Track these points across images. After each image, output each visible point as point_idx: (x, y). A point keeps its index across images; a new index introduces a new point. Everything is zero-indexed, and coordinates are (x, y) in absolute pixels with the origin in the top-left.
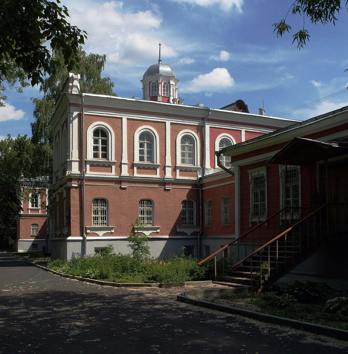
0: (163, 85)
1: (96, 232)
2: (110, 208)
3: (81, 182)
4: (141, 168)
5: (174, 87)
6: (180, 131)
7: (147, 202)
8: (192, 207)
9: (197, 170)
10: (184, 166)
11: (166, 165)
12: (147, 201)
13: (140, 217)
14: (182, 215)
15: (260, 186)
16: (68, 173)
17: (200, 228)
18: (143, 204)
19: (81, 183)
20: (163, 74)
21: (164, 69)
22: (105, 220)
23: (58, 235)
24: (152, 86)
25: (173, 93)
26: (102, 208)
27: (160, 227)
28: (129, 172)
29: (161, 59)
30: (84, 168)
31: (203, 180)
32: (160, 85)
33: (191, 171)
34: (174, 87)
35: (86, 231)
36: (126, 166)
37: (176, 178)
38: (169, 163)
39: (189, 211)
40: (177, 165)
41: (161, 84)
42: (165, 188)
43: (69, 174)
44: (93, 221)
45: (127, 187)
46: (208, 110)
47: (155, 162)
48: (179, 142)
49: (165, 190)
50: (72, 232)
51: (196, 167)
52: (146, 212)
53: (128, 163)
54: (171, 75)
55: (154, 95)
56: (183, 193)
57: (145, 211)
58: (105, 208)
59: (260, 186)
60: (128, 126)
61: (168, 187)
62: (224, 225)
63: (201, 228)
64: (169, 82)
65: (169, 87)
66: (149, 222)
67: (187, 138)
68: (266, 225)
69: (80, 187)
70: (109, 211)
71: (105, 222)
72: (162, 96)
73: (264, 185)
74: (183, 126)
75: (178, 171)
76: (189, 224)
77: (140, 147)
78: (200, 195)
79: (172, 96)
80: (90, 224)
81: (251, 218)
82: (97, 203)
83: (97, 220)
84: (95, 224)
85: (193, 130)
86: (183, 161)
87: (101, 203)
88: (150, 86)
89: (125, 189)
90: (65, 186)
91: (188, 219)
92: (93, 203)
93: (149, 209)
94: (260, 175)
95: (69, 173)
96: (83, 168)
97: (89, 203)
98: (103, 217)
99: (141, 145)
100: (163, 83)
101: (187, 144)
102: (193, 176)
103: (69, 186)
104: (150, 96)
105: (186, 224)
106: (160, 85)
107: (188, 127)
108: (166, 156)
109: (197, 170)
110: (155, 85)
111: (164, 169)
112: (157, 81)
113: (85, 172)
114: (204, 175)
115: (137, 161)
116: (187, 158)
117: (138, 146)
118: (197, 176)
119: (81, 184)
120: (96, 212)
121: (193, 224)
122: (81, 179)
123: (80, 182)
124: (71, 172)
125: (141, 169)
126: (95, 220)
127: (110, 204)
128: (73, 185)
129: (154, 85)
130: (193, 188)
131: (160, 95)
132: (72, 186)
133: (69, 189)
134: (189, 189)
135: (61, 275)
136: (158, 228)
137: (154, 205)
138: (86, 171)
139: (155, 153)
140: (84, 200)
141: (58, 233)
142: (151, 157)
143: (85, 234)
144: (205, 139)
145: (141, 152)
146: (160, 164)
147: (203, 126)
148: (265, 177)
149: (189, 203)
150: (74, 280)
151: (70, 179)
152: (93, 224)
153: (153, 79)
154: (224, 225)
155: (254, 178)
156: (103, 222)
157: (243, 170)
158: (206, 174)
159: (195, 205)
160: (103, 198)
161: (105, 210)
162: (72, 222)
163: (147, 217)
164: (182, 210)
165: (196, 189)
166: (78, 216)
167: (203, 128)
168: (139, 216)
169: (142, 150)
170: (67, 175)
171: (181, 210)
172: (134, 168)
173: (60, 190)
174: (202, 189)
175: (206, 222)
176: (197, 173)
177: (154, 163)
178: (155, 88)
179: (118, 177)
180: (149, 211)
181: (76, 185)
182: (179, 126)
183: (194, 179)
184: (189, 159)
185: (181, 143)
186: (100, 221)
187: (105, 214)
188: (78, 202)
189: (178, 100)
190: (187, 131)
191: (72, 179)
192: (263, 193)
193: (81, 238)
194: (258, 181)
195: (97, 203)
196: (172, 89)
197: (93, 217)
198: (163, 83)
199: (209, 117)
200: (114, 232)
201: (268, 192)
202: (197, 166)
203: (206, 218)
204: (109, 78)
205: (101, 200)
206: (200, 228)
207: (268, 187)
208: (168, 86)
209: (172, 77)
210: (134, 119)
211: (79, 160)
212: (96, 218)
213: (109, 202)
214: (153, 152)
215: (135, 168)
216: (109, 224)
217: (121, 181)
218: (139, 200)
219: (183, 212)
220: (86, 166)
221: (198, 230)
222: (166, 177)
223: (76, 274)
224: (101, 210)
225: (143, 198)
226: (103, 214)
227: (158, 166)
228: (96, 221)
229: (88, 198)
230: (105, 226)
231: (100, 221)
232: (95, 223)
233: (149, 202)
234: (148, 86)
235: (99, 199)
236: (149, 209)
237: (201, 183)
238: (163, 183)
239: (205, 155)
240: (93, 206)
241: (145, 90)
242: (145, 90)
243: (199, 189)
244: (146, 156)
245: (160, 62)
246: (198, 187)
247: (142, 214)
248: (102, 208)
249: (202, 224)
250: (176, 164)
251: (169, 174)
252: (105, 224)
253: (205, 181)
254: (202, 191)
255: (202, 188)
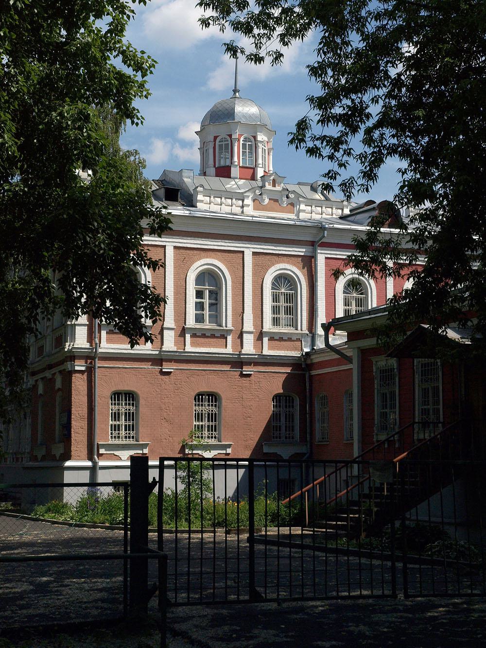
0: (241, 142)
1: (116, 453)
2: (141, 409)
3: (92, 362)
4: (197, 335)
5: (266, 145)
6: (270, 267)
7: (209, 398)
8: (293, 407)
9: (301, 338)
10: (277, 331)
11: (243, 330)
12: (209, 395)
13: (195, 425)
14: (274, 421)
15: (389, 383)
16: (67, 346)
17: (307, 445)
18: (202, 401)
19: (91, 363)
20: (243, 121)
21: (245, 109)
22: (133, 430)
23: (39, 457)
24: (221, 146)
25: (264, 158)
26: (126, 409)
27: (231, 443)
28: (176, 343)
29: (238, 88)
30: (97, 336)
31: (312, 357)
32: (236, 144)
33: (290, 340)
34: (266, 145)
35: (98, 451)
36: (172, 333)
37: (262, 353)
38: (249, 325)
39: (286, 414)
40: (264, 330)
41: (239, 140)
42: (241, 372)
43: (70, 348)
44: (110, 432)
45: (172, 370)
46: (321, 228)
47: (224, 325)
48: (268, 286)
49: (242, 375)
50: (72, 453)
51: (299, 331)
52: (206, 415)
53: (175, 327)
54: (259, 123)
55: (222, 164)
56: (274, 382)
57: (205, 414)
58: (132, 409)
59: (389, 383)
60: (176, 260)
61: (247, 370)
62: (348, 442)
63: (308, 446)
64: (255, 137)
65: (256, 147)
66: (212, 434)
67: (283, 279)
68: (386, 446)
69: (90, 372)
70: (141, 415)
71: (132, 434)
72: (240, 167)
73: (394, 383)
74: (275, 257)
75: (265, 340)
76: (286, 438)
77: (196, 298)
78: (307, 384)
79: (261, 166)
80: (103, 437)
81: (377, 435)
82: (119, 400)
83: (119, 430)
84: (115, 437)
85: (294, 265)
86: (276, 322)
87: (126, 400)
88: (215, 144)
89: (169, 373)
90: (61, 368)
91: (283, 428)
92: (112, 401)
93: (212, 411)
94: (388, 366)
95: (69, 346)
96: (95, 337)
97: (103, 399)
98: (129, 425)
99: (199, 294)
100: (242, 139)
101: (283, 291)
102: (295, 349)
103: (70, 369)
104: (215, 166)
105: (280, 438)
106: (236, 144)
107: (285, 258)
108: (243, 313)
109: (301, 338)
110: (226, 143)
111: (241, 336)
112: (230, 136)
113: (98, 344)
114: (315, 348)
115: (191, 323)
116: (282, 315)
117: (193, 297)
118: (302, 350)
119: (90, 365)
120: (116, 416)
121: (293, 438)
122: (90, 357)
123: (89, 361)
124: (73, 345)
125: (199, 337)
126: (115, 430)
127: (142, 402)
128: (77, 368)
129: (224, 143)
130: (293, 372)
131: (236, 163)
132: (76, 369)
133: (68, 376)
134: (287, 373)
135: (70, 525)
136: (229, 446)
137: (220, 403)
138: (100, 343)
139: (224, 308)
140: (97, 396)
141: (40, 453)
142: (217, 315)
143: (96, 457)
144: (316, 281)
145: (200, 306)
146: (232, 328)
147: (313, 257)
148: (396, 370)
149: (286, 399)
150: (97, 529)
151: (72, 356)
152: (110, 437)
153: (220, 130)
154: (348, 442)
155: (380, 370)
156: (129, 433)
157: (365, 355)
158: (318, 345)
159: (297, 402)
160: (130, 391)
161: (133, 413)
162: (73, 435)
163: (208, 426)
164: (273, 411)
165: (300, 372)
166: (84, 424)
167: (313, 260)
168: (195, 423)
169: (200, 303)
170: (66, 350)
171: (271, 413)
172: (185, 335)
173: (48, 374)
174: (310, 373)
175: (318, 436)
176: (302, 344)
177: (221, 326)
178: (228, 147)
179: (157, 352)
180: (212, 414)
181: (83, 368)
182: (268, 257)
183: (297, 354)
184: (287, 318)
185: (273, 288)
186: (123, 433)
187: (133, 420)
188: (85, 399)
189: (272, 178)
190: (284, 267)
191: (74, 356)
192: (393, 394)
193: (89, 464)
194: (387, 375)
195: (119, 400)
196: (260, 151)
197: (112, 425)
198: (242, 139)
199: (324, 240)
200: (147, 452)
201: (400, 394)
202: (302, 330)
203: (317, 426)
204: (136, 151)
205: (126, 394)
206: (307, 445)
207: (400, 387)
208: (252, 146)
209: (263, 127)
210: (187, 247)
211: (88, 323)
212: (116, 428)
213: (141, 399)
214: (220, 318)
215: (188, 336)
216: (140, 437)
217: (162, 359)
218: (194, 394)
219: (275, 417)
220: (100, 333)
221: (303, 449)
222: (243, 352)
223: (98, 521)
224: (126, 413)
225: (202, 390)
226: (129, 420)
227: (229, 332)
228: (115, 433)
229: (103, 392)
230: (131, 442)
231: (123, 433)
232: (113, 435)
233: (213, 397)
234: (212, 145)
235: (121, 393)
236: (212, 411)
237: (309, 362)
238: (238, 363)
239: (317, 311)
240: (112, 405)
241: (205, 151)
242: (205, 151)
243: (304, 372)
244: (207, 313)
245: (237, 94)
246: (303, 369)
247: (198, 421)
248: (126, 409)
249: (311, 439)
250: (262, 328)
251: (249, 347)
252: (133, 437)
253: (316, 359)
254: (311, 377)
255: (311, 372)
